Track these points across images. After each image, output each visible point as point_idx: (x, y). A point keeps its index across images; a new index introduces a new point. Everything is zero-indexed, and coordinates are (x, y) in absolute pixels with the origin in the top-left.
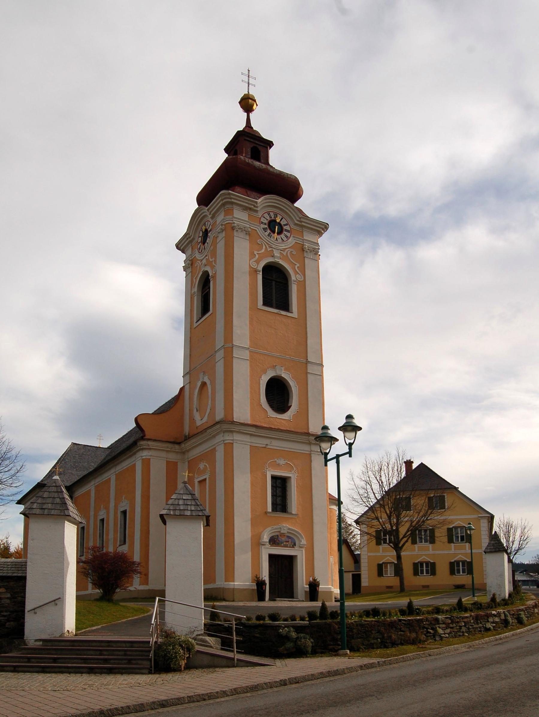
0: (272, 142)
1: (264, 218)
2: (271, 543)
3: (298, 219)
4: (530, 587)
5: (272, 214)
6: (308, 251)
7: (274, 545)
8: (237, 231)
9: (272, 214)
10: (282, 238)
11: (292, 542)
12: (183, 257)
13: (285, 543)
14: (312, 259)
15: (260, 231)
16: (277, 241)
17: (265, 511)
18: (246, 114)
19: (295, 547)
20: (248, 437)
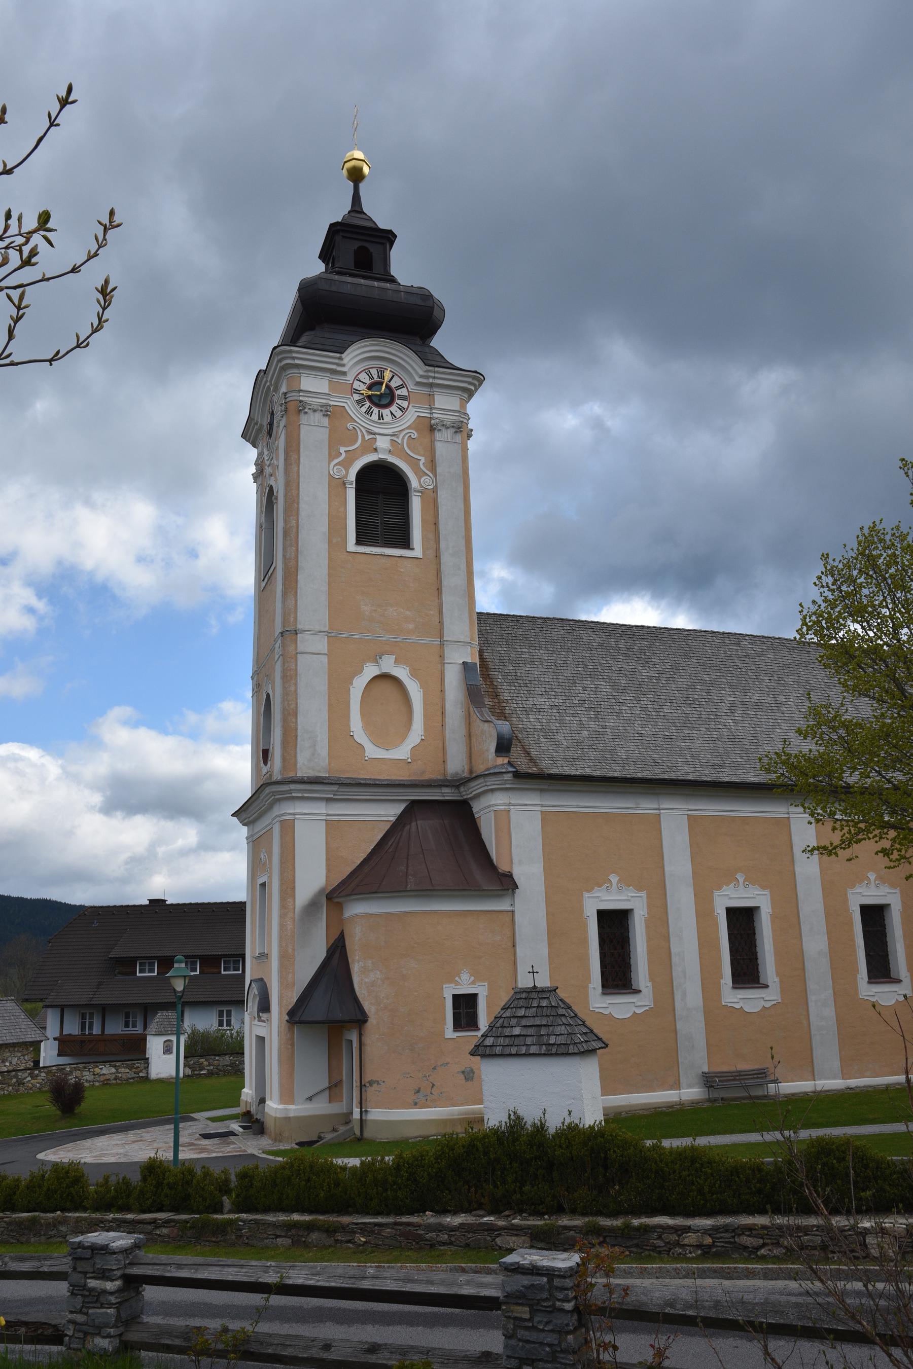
1: (360, 381)
5: (374, 372)
6: (443, 429)
10: (392, 413)
15: (349, 405)
16: (383, 419)
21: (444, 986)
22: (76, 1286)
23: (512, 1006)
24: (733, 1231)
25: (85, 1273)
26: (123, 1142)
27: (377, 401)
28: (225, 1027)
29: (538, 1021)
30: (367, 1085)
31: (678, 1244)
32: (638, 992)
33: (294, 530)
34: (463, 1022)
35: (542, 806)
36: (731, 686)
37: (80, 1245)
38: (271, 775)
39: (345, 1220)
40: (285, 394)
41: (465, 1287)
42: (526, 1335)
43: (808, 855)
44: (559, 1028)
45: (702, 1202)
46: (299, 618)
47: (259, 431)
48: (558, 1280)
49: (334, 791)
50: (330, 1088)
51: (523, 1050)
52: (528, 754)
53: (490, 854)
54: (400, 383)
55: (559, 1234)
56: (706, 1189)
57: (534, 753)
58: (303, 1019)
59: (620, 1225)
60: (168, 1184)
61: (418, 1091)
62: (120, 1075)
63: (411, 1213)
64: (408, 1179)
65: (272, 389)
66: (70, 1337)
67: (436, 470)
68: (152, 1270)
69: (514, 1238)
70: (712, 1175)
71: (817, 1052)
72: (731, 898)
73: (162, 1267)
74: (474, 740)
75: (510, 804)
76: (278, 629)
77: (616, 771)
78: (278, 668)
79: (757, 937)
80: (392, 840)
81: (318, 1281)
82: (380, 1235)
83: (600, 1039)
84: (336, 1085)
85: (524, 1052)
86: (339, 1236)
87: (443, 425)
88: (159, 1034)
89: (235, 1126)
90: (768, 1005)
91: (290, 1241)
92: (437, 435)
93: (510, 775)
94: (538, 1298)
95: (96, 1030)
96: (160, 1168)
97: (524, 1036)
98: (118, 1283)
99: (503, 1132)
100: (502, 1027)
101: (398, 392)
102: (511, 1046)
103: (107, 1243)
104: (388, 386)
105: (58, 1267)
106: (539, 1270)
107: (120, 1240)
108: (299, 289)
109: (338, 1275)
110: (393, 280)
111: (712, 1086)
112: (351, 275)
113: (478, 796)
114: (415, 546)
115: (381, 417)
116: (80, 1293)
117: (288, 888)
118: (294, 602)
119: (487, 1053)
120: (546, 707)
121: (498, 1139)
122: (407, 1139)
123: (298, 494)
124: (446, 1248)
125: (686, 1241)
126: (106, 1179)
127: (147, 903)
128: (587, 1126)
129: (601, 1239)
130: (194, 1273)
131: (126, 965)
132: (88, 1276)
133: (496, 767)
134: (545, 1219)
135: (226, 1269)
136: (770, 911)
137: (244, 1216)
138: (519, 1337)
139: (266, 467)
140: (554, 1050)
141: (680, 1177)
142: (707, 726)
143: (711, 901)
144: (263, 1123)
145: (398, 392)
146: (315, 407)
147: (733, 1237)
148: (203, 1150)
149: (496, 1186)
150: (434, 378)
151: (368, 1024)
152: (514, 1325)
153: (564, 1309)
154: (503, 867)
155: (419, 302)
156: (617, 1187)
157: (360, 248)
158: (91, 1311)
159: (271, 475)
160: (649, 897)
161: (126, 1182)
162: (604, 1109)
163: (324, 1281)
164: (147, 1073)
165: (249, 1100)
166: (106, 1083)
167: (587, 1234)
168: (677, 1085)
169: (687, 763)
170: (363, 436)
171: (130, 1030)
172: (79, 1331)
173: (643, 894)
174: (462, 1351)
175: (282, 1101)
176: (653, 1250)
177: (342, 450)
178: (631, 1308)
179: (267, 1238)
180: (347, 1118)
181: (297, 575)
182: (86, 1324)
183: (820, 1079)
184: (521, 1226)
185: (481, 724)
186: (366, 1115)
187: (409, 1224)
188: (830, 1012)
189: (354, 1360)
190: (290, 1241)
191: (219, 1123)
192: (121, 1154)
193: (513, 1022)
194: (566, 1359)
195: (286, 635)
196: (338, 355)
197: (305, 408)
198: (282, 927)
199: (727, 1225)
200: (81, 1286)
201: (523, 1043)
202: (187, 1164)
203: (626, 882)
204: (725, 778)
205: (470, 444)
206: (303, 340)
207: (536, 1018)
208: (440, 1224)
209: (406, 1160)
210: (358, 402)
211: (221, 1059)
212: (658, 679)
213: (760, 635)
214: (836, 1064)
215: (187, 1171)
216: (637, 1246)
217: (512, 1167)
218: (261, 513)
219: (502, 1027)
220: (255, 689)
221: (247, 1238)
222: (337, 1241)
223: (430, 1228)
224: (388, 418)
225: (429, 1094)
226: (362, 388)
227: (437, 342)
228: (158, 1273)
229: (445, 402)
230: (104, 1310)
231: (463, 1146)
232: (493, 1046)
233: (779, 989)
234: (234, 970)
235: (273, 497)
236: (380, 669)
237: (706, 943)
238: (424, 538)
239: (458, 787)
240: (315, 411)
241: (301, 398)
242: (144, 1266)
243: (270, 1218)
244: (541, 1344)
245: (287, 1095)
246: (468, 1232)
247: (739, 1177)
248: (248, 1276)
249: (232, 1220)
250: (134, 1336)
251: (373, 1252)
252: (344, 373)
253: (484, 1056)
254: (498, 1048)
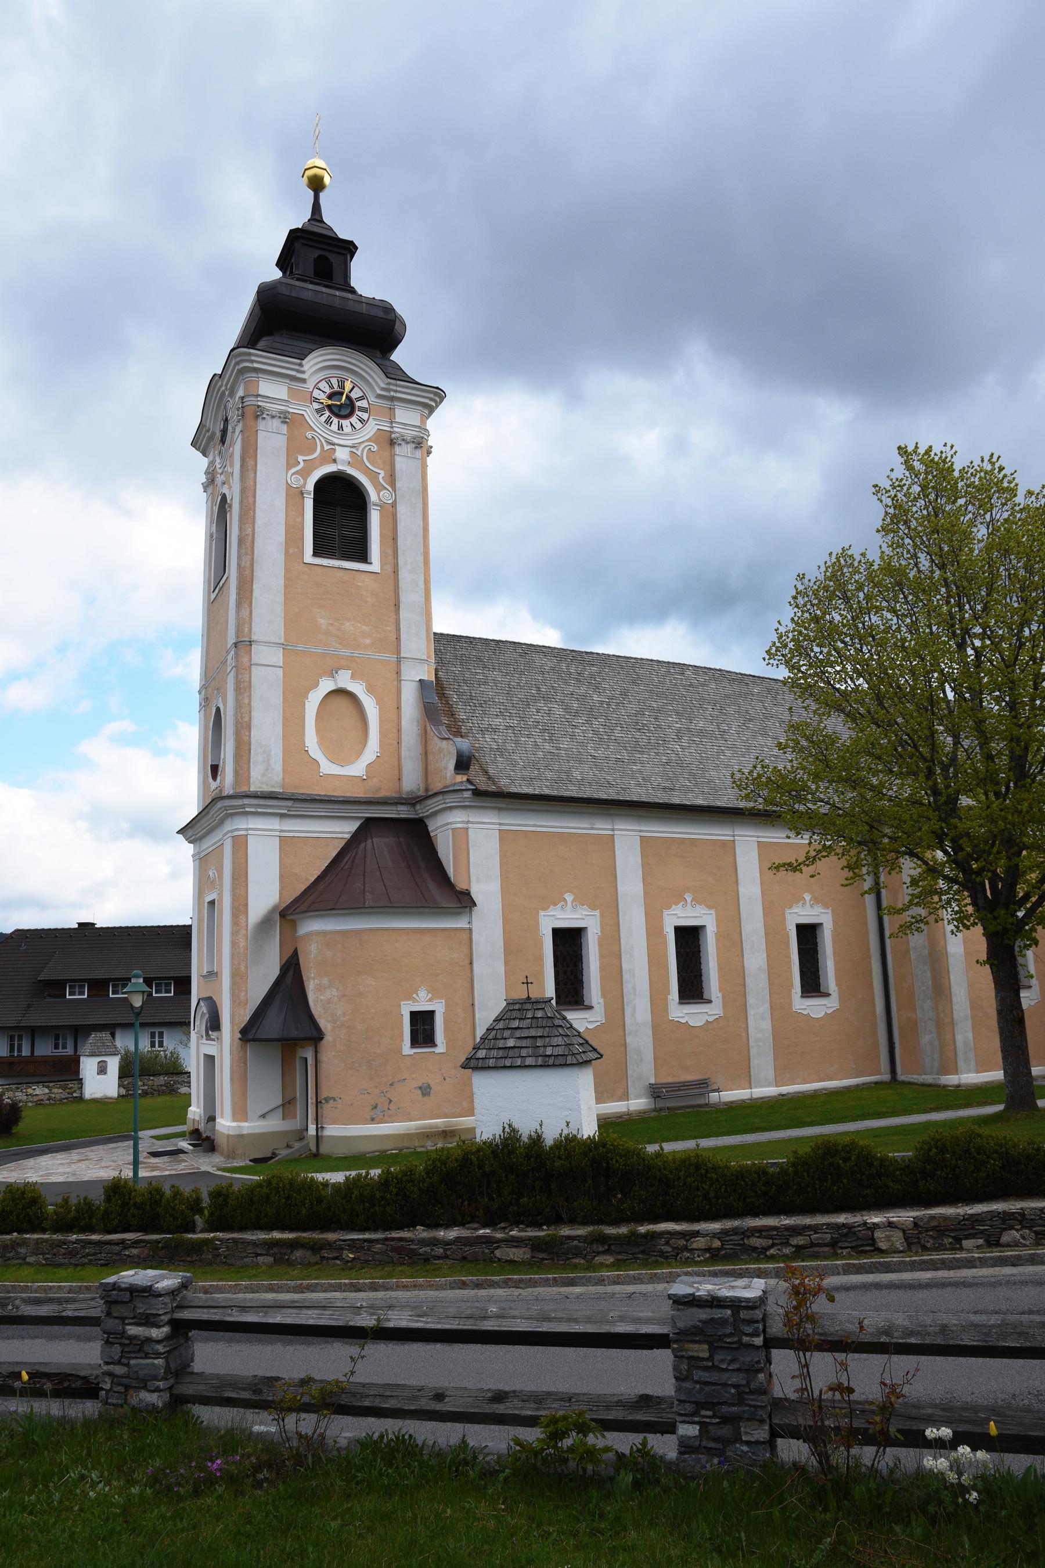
0: (351, 243)
4: (367, 1174)
5: (334, 381)
6: (403, 443)
9: (334, 381)
10: (352, 425)
12: (203, 462)
18: (312, 193)
21: (402, 1003)
22: (112, 1334)
23: (504, 1018)
24: (743, 1233)
25: (123, 1319)
26: (68, 1161)
27: (337, 412)
28: (157, 1048)
29: (533, 1033)
30: (323, 1101)
31: (686, 1248)
32: (591, 1008)
33: (250, 538)
34: (420, 1039)
35: (500, 824)
36: (677, 714)
37: (115, 1286)
38: (221, 791)
39: (331, 1236)
40: (242, 398)
41: (618, 1324)
42: (705, 1376)
43: (774, 871)
44: (556, 1039)
45: (707, 1207)
46: (253, 629)
47: (211, 438)
48: (745, 1312)
49: (287, 807)
50: (283, 1105)
51: (518, 1062)
52: (486, 772)
53: (448, 872)
54: (361, 394)
55: (562, 1244)
56: (712, 1194)
57: (491, 772)
58: (257, 1036)
59: (626, 1232)
60: (135, 1204)
61: (376, 1107)
62: (53, 1096)
63: (401, 1228)
64: (397, 1195)
65: (227, 393)
66: (107, 1391)
67: (395, 484)
68: (208, 1314)
69: (514, 1250)
70: (717, 1180)
71: (754, 1062)
72: (678, 917)
73: (221, 1311)
74: (430, 758)
75: (468, 822)
76: (231, 639)
77: (573, 792)
78: (231, 680)
79: (702, 954)
80: (348, 857)
81: (427, 1323)
82: (370, 1250)
83: (595, 1050)
84: (289, 1102)
85: (519, 1064)
86: (325, 1253)
87: (403, 440)
88: (93, 1055)
89: (184, 1144)
90: (711, 1019)
91: (272, 1259)
92: (397, 450)
93: (470, 793)
94: (720, 1333)
95: (26, 1052)
96: (125, 1187)
97: (518, 1047)
98: (166, 1330)
99: (497, 1145)
100: (495, 1039)
101: (358, 404)
102: (505, 1058)
103: (149, 1284)
105: (85, 1311)
106: (721, 1301)
107: (166, 1280)
108: (258, 292)
109: (452, 1315)
110: (353, 291)
111: (659, 1097)
112: (312, 283)
113: (435, 814)
114: (373, 561)
115: (340, 427)
116: (117, 1341)
117: (240, 906)
118: (248, 612)
119: (480, 1065)
120: (501, 727)
121: (493, 1152)
122: (365, 1154)
123: (255, 501)
124: (441, 1261)
125: (695, 1246)
126: (66, 1201)
127: (76, 926)
128: (585, 1137)
129: (606, 1247)
130: (263, 1317)
131: (56, 987)
132: (126, 1322)
133: (455, 784)
134: (543, 1230)
135: (305, 1311)
136: (715, 930)
137: (220, 1235)
138: (695, 1379)
139: (218, 476)
140: (551, 1062)
141: (685, 1183)
142: (656, 751)
143: (661, 919)
144: (213, 1141)
145: (358, 404)
146: (274, 413)
147: (742, 1239)
148: (154, 1168)
149: (491, 1199)
150: (396, 391)
151: (324, 1042)
152: (688, 1365)
153: (753, 1345)
154: (461, 885)
155: (381, 314)
156: (619, 1196)
157: (320, 256)
158: (132, 1362)
159: (224, 483)
160: (602, 915)
161: (88, 1203)
162: (598, 1115)
163: (434, 1323)
164: (81, 1093)
165: (197, 1118)
166: (39, 1103)
167: (591, 1243)
168: (625, 1097)
169: (639, 785)
170: (322, 446)
171: (60, 1052)
172: (119, 1385)
173: (597, 913)
174: (614, 1395)
175: (235, 1119)
176: (660, 1256)
177: (301, 458)
178: (836, 1339)
179: (246, 1257)
180: (301, 1134)
181: (252, 585)
182: (127, 1376)
183: (756, 1087)
184: (521, 1237)
185: (438, 741)
186: (322, 1131)
187: (400, 1239)
188: (767, 1025)
189: (477, 1410)
190: (272, 1259)
191: (165, 1141)
192: (68, 1173)
193: (507, 1033)
194: (757, 1401)
195: (240, 646)
196: (298, 361)
197: (263, 413)
198: (234, 944)
199: (736, 1228)
200: (119, 1334)
201: (517, 1055)
202: (154, 1184)
203: (581, 900)
204: (676, 801)
205: (430, 460)
206: (261, 344)
207: (531, 1030)
208: (435, 1239)
209: (395, 1175)
210: (318, 411)
211: (156, 1079)
212: (608, 704)
213: (703, 666)
214: (771, 1073)
215: (155, 1191)
216: (643, 1252)
217: (507, 1180)
218: (211, 522)
219: (495, 1039)
220: (203, 704)
221: (225, 1257)
222: (323, 1258)
223: (423, 1242)
224: (347, 429)
225: (386, 1109)
226: (322, 397)
227: (398, 356)
228: (217, 1318)
229: (406, 416)
230: (150, 1361)
231: (457, 1160)
232: (486, 1058)
233: (721, 1004)
234: (166, 993)
235: (227, 506)
236: (336, 684)
237: (655, 961)
238: (383, 553)
239: (413, 805)
240: (273, 417)
241: (260, 403)
242: (197, 1310)
243: (249, 1236)
244: (725, 1385)
245: (240, 1112)
246: (465, 1245)
247: (744, 1181)
248: (334, 1319)
249: (208, 1239)
250: (187, 1389)
251: (363, 1268)
252: (304, 381)
253: (476, 1068)
254: (491, 1060)
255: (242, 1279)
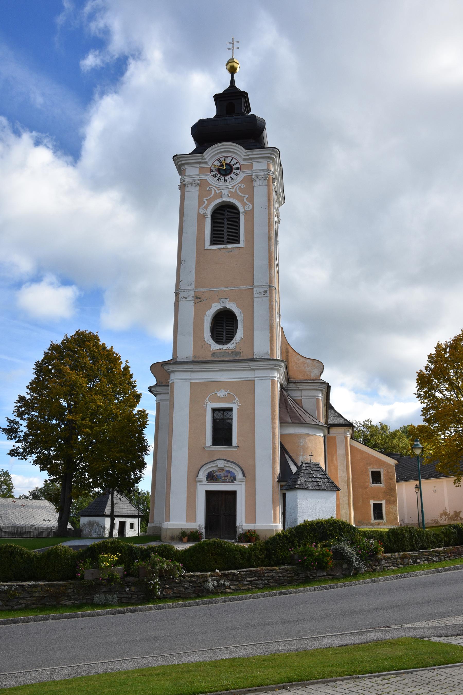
2: (209, 479)
3: (245, 154)
6: (257, 180)
7: (212, 481)
8: (188, 186)
10: (231, 178)
11: (231, 477)
13: (223, 478)
14: (261, 185)
17: (203, 446)
18: (231, 75)
19: (234, 482)
20: (189, 373)
101: (234, 167)
104: (227, 164)
113: (173, 372)
115: (226, 180)
145: (234, 167)
252: (206, 162)
255: (186, 601)
